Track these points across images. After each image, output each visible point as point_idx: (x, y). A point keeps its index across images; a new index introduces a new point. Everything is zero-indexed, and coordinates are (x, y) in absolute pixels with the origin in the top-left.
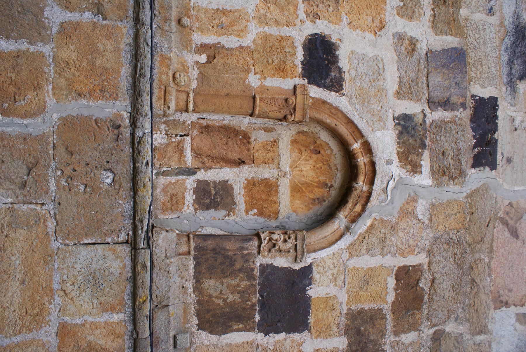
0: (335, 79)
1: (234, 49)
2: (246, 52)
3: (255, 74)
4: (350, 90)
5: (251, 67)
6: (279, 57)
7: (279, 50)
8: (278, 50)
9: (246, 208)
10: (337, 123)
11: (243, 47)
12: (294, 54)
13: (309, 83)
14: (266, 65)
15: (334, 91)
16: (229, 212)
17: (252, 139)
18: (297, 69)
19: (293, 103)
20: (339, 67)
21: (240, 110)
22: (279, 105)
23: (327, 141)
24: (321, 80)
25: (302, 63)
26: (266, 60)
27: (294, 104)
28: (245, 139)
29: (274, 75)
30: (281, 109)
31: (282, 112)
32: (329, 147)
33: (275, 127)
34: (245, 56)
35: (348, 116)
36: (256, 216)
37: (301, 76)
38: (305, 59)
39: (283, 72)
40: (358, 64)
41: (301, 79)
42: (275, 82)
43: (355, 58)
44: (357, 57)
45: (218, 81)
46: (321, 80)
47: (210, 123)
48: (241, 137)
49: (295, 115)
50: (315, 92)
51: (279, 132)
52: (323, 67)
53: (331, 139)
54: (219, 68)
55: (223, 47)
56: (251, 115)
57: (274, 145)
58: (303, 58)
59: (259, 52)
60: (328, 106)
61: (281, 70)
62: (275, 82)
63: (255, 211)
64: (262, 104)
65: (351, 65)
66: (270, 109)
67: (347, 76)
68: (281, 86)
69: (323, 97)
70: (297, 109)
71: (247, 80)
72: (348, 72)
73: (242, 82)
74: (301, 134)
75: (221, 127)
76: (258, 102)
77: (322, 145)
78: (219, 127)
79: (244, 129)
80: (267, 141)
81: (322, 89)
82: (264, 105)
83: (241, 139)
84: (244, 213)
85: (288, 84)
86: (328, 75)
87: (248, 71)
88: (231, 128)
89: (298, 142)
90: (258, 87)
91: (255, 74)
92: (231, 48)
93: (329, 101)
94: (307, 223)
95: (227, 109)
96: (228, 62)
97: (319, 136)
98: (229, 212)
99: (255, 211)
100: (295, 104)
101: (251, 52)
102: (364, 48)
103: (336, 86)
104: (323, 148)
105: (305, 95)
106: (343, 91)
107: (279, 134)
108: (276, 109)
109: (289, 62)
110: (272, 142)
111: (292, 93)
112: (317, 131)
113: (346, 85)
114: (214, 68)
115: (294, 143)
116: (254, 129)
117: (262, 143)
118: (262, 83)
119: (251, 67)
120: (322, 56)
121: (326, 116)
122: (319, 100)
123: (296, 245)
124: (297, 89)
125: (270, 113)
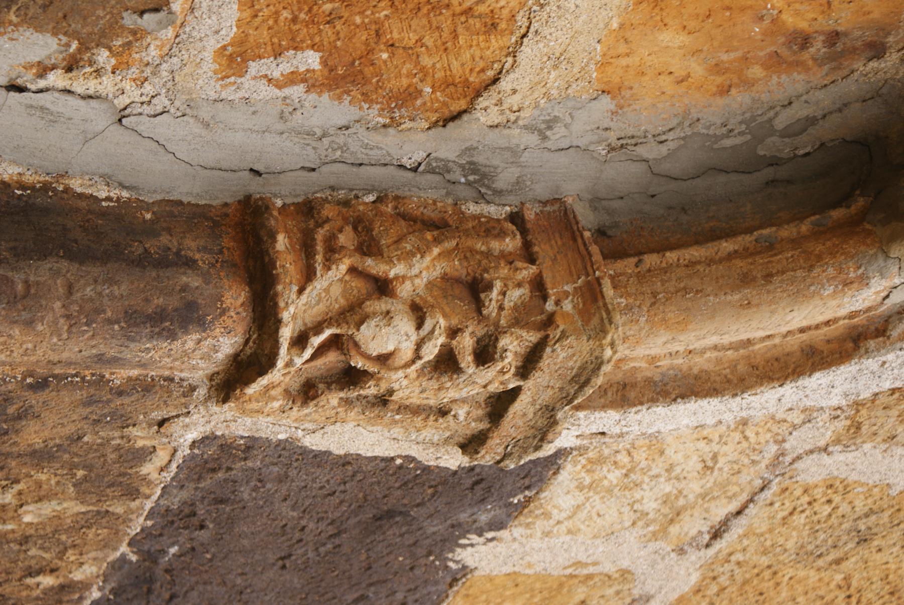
9: (241, 41)
16: (84, 47)
36: (297, 91)
63: (311, 60)
84: (209, 66)
94: (666, 167)
98: (84, 47)
99: (311, 60)
123: (513, 394)
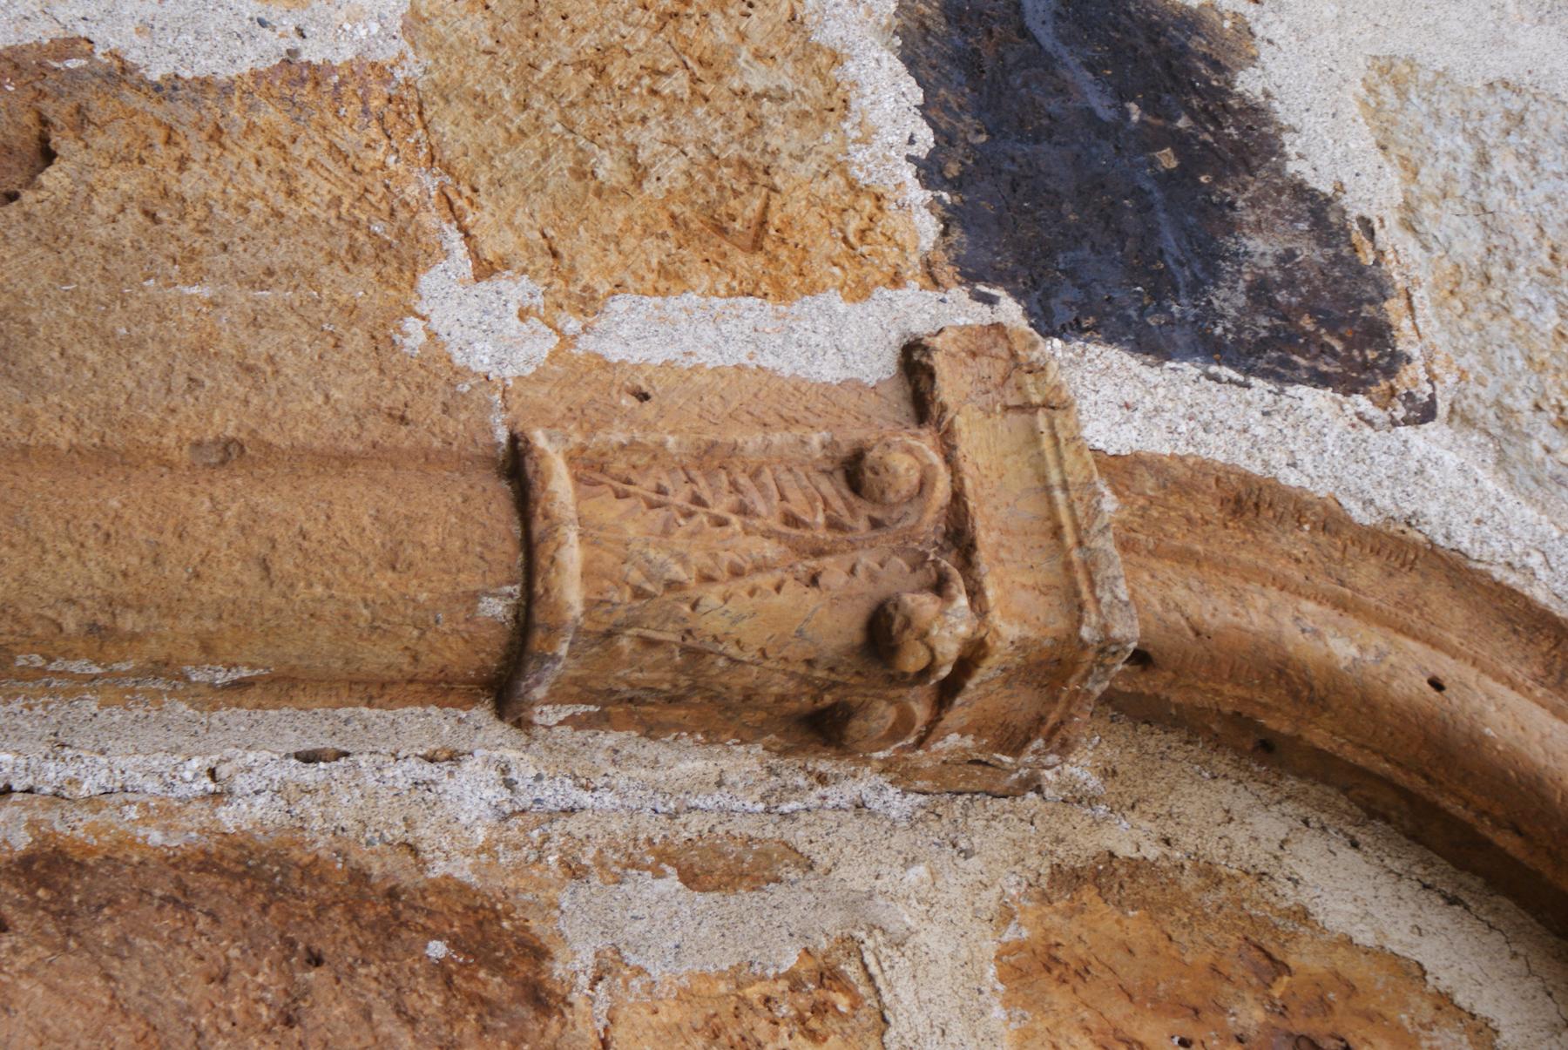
0: (1290, 283)
1: (226, 90)
2: (351, 110)
3: (485, 269)
4: (1469, 360)
5: (431, 219)
6: (690, 132)
7: (678, 83)
8: (666, 86)
10: (1446, 667)
11: (316, 75)
12: (836, 105)
13: (1047, 324)
14: (577, 203)
15: (1321, 380)
17: (573, 962)
18: (892, 220)
19: (924, 485)
20: (1300, 190)
21: (384, 580)
22: (791, 520)
23: (1399, 939)
24: (1156, 294)
25: (929, 171)
26: (562, 162)
27: (941, 491)
28: (496, 967)
29: (670, 277)
30: (818, 553)
31: (834, 572)
32: (1444, 1001)
33: (798, 836)
34: (348, 139)
35: (1540, 595)
37: (946, 272)
38: (946, 138)
39: (756, 246)
40: (1484, 161)
41: (959, 294)
42: (686, 335)
43: (1437, 116)
44: (1447, 106)
45: (107, 339)
46: (1156, 294)
47: (75, 827)
48: (437, 949)
49: (975, 593)
50: (1129, 403)
51: (855, 876)
52: (1138, 193)
53: (1437, 916)
54: (102, 233)
55: (121, 73)
56: (502, 687)
57: (821, 1009)
58: (926, 139)
59: (483, 105)
60: (1298, 541)
61: (737, 232)
62: (686, 335)
64: (608, 510)
65: (1411, 170)
66: (698, 557)
67: (1402, 256)
68: (769, 361)
69: (1217, 449)
70: (986, 538)
71: (411, 324)
72: (1409, 226)
73: (357, 340)
74: (1088, 894)
75: (207, 863)
76: (560, 486)
77: (1351, 989)
78: (175, 862)
79: (463, 870)
80: (738, 977)
81: (1190, 369)
82: (631, 524)
83: (442, 973)
85: (836, 342)
86: (1210, 259)
87: (403, 257)
88: (313, 871)
89: (1083, 972)
90: (539, 378)
91: (485, 269)
92: (205, 83)
93: (1292, 479)
95: (252, 577)
96: (189, 185)
97: (1291, 897)
100: (958, 496)
101: (405, 110)
102: (1498, 42)
103: (1331, 327)
104: (1370, 1017)
105: (1026, 408)
106: (1412, 377)
107: (854, 903)
108: (770, 549)
109: (804, 171)
110: (795, 983)
111: (897, 401)
112: (1261, 860)
113: (1424, 331)
114: (55, 239)
115: (1044, 981)
116: (574, 871)
117: (685, 996)
118: (567, 341)
119: (431, 219)
120: (1106, 114)
121: (1309, 606)
122: (1185, 488)
124: (939, 362)
125: (712, 597)
